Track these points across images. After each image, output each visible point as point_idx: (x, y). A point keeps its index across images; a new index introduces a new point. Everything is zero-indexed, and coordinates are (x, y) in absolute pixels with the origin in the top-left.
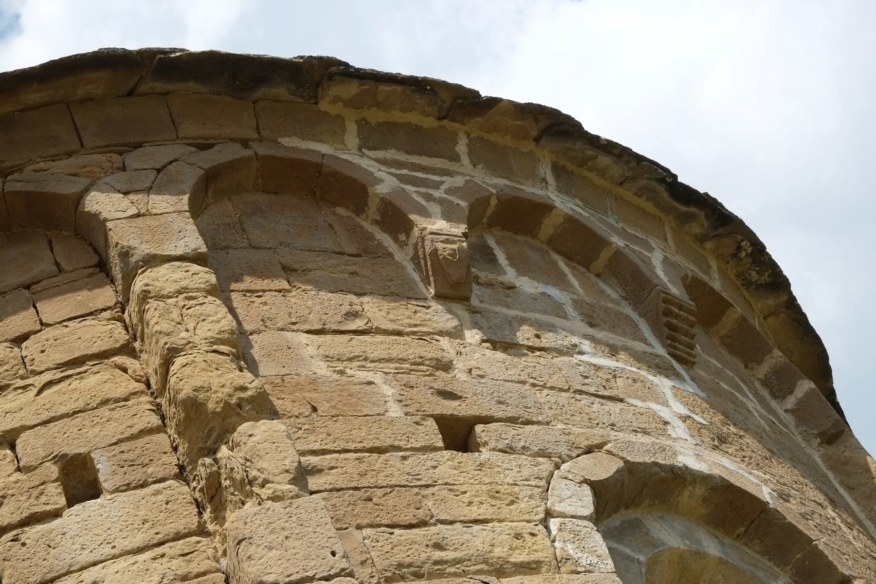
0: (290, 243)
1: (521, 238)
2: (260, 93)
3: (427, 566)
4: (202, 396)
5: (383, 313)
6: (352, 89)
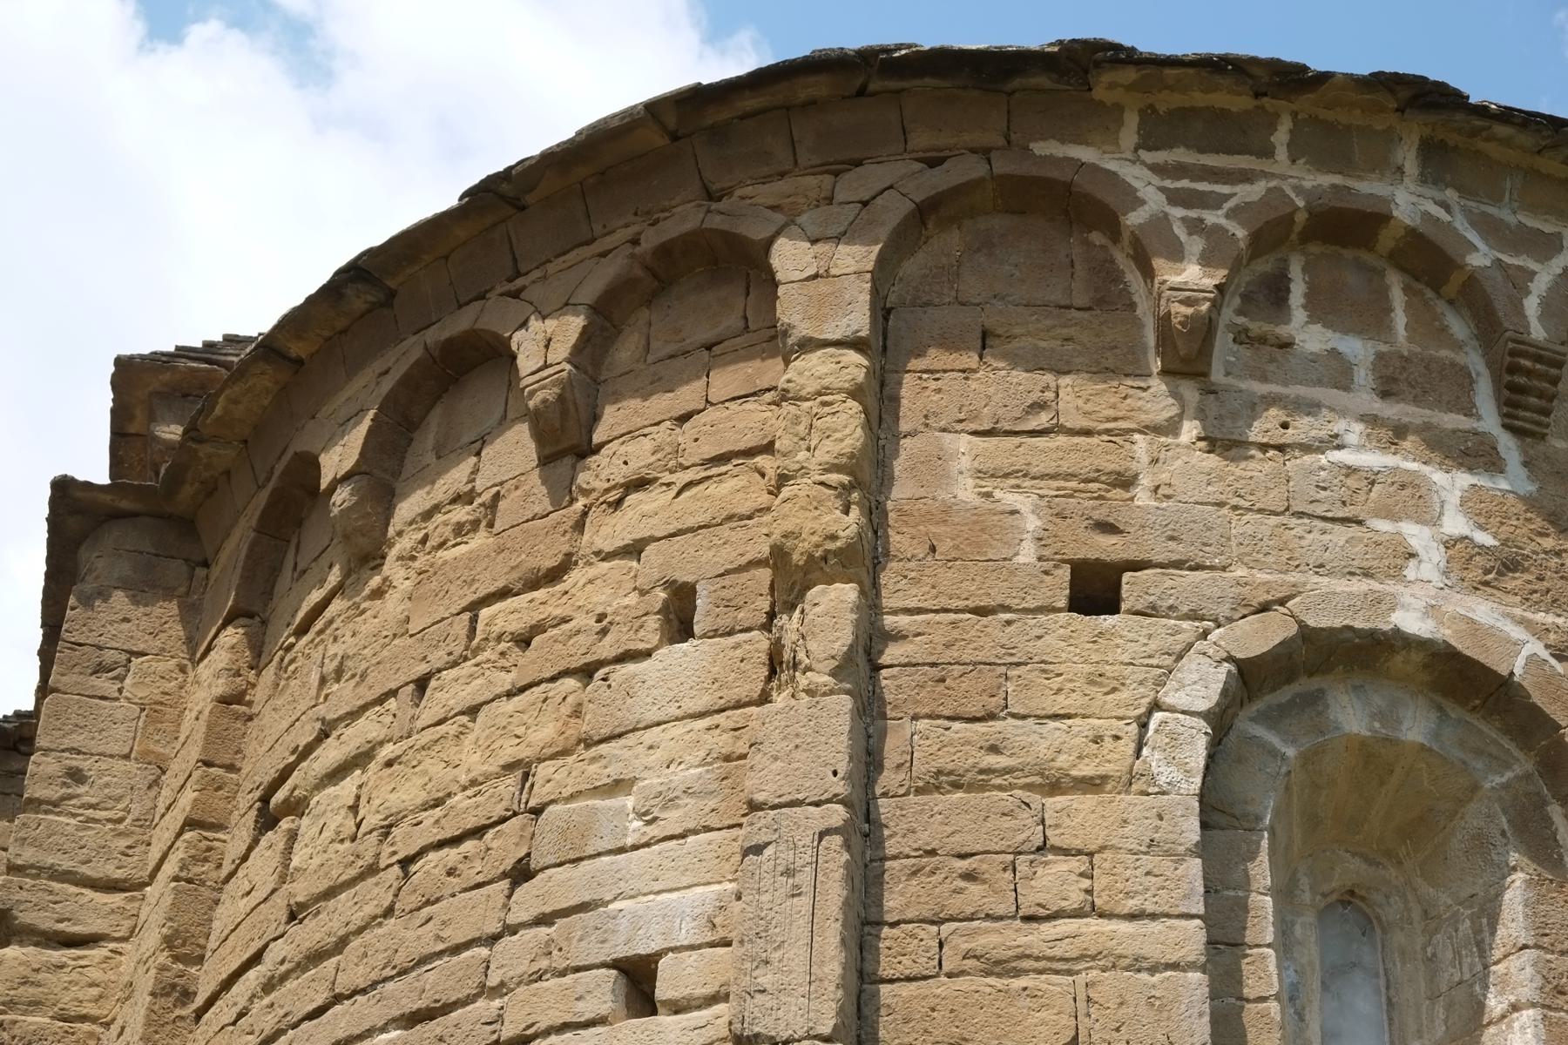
0: (1007, 295)
1: (1348, 254)
2: (1016, 83)
3: (969, 775)
4: (789, 543)
5: (1080, 402)
6: (1130, 75)
